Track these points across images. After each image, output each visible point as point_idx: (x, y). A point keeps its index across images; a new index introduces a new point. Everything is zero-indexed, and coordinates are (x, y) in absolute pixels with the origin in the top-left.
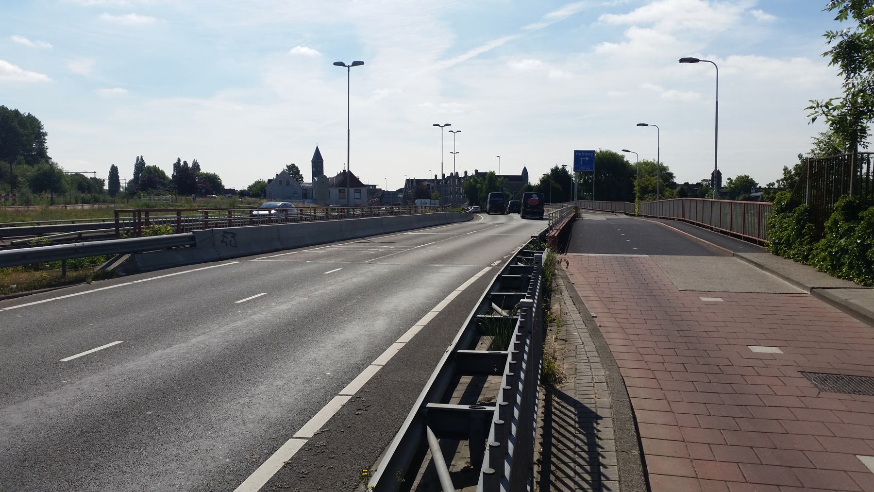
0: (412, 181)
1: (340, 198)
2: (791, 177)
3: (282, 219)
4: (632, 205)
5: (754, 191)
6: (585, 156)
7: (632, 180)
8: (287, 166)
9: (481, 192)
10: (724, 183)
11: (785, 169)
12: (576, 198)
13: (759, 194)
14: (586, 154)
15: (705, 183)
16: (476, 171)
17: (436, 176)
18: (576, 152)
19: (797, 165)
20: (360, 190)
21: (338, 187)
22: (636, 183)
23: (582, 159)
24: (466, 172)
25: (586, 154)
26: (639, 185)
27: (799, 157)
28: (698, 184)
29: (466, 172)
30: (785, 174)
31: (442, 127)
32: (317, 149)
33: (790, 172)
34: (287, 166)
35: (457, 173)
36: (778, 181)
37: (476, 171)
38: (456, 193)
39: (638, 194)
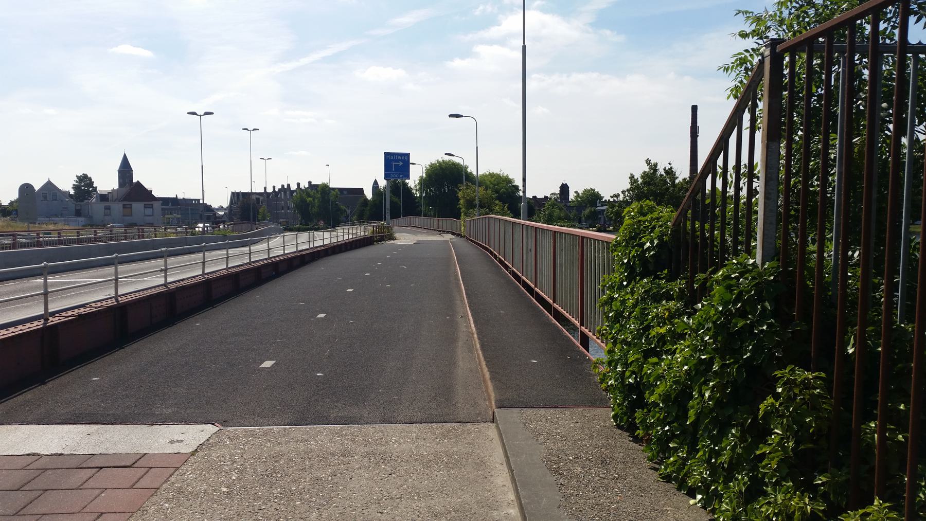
0: (238, 194)
1: (124, 215)
2: (638, 187)
3: (70, 239)
4: (458, 223)
5: (600, 205)
6: (398, 161)
7: (456, 191)
8: (77, 176)
9: (312, 207)
10: (572, 196)
11: (632, 177)
12: (388, 216)
13: (605, 207)
14: (399, 158)
15: (553, 197)
16: (310, 183)
17: (265, 188)
18: (386, 154)
19: (644, 173)
20: (152, 205)
21: (122, 201)
22: (460, 194)
23: (394, 163)
24: (298, 184)
25: (399, 158)
26: (464, 197)
27: (646, 162)
28: (546, 197)
29: (298, 184)
30: (631, 183)
31: (201, 115)
32: (125, 155)
33: (636, 181)
34: (77, 176)
35: (289, 185)
36: (623, 192)
37: (310, 183)
38: (288, 208)
39: (463, 209)
